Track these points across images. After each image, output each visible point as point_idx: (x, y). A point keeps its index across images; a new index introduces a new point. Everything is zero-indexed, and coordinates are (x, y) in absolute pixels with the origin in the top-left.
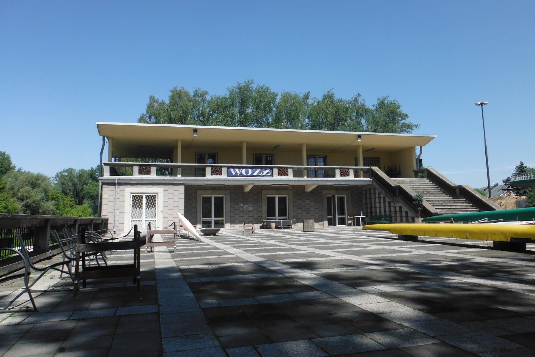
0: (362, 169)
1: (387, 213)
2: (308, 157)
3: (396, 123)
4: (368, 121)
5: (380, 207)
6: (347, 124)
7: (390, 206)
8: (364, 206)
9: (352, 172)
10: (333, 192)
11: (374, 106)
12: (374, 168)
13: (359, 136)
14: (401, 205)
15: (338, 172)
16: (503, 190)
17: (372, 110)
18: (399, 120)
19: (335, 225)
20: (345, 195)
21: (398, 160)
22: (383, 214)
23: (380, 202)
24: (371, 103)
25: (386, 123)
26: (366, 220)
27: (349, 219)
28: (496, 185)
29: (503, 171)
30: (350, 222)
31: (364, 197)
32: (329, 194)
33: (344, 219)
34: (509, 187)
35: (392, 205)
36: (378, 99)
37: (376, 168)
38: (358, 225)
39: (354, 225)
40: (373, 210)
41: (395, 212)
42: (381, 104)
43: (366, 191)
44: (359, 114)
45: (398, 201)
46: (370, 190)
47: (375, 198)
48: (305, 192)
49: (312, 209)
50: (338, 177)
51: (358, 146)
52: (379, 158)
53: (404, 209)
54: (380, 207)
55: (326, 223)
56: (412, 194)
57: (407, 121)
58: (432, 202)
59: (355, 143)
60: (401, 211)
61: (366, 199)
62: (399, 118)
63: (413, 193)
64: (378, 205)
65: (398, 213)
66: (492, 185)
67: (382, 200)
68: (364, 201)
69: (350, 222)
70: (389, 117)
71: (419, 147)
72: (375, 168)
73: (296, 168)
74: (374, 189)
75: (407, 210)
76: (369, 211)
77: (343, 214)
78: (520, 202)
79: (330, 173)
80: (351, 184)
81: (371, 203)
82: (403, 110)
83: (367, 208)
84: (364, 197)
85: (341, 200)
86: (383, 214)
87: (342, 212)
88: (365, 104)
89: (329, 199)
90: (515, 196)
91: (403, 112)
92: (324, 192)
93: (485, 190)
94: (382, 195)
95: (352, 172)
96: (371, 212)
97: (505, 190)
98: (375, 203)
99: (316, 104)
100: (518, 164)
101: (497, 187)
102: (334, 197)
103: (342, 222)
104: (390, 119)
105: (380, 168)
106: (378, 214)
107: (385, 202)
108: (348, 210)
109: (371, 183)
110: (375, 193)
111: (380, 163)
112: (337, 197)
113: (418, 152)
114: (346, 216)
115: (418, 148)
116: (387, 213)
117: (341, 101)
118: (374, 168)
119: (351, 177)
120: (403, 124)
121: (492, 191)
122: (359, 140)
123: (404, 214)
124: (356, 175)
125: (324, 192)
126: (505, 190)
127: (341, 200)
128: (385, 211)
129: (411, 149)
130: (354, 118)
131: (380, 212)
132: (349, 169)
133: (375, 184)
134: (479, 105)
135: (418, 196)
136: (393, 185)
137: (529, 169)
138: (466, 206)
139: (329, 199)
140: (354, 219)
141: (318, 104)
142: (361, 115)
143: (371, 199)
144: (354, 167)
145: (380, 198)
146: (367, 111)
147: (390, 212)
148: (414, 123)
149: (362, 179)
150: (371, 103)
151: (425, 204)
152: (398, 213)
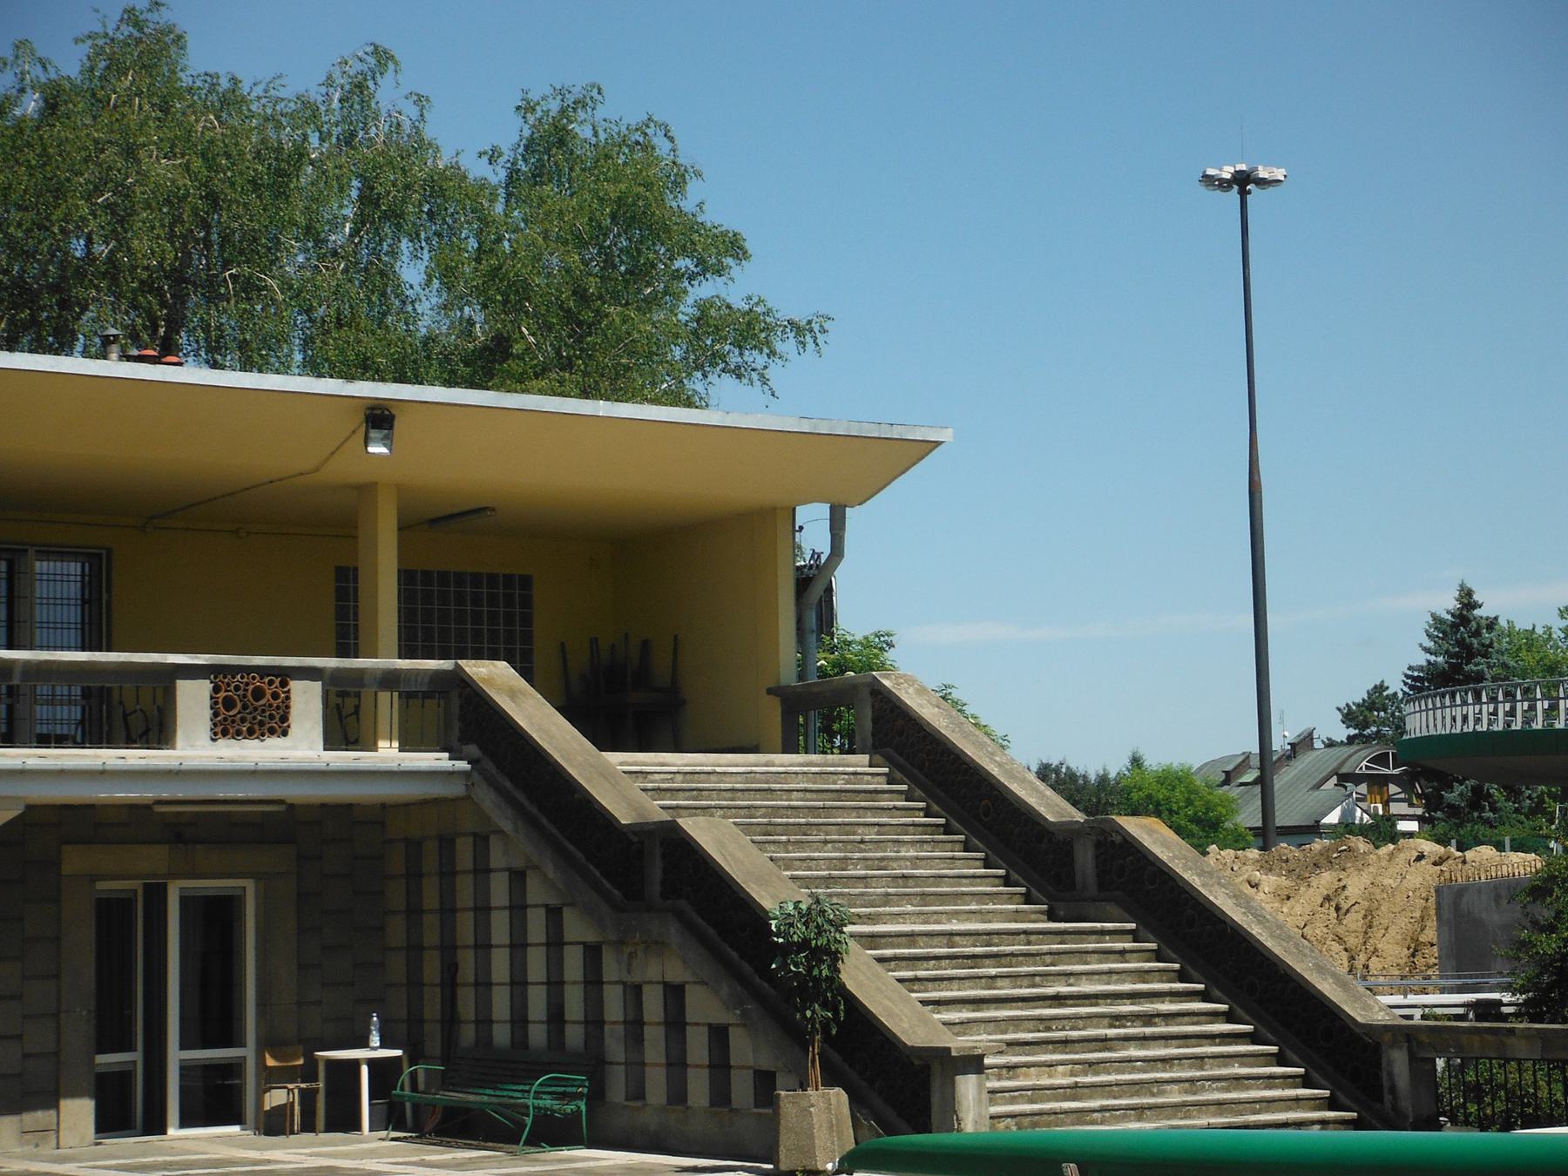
0: (390, 680)
1: (574, 1036)
2: (210, 1069)
3: (652, 302)
4: (445, 273)
5: (519, 983)
6: (286, 285)
7: (593, 981)
8: (397, 968)
9: (306, 701)
10: (153, 858)
11: (493, 156)
12: (480, 670)
13: (379, 418)
14: (675, 972)
15: (193, 699)
16: (1344, 778)
17: (482, 185)
18: (677, 276)
19: (156, 1125)
20: (249, 885)
21: (670, 613)
22: (538, 1035)
23: (518, 946)
24: (473, 135)
25: (581, 294)
26: (403, 1089)
27: (271, 1079)
28: (1304, 743)
29: (1354, 644)
30: (276, 1097)
31: (397, 896)
32: (119, 873)
33: (233, 1069)
34: (1381, 760)
35: (611, 968)
36: (526, 108)
38: (344, 1121)
39: (308, 1126)
41: (635, 1026)
42: (549, 146)
43: (414, 847)
44: (379, 213)
45: (657, 946)
46: (447, 843)
47: (483, 910)
50: (196, 746)
51: (365, 491)
52: (526, 582)
53: (703, 1006)
54: (519, 983)
55: (79, 1112)
56: (767, 903)
57: (734, 289)
58: (898, 955)
59: (345, 469)
60: (676, 1023)
61: (414, 912)
62: (682, 263)
63: (774, 891)
65: (654, 1036)
66: (1279, 744)
67: (536, 929)
68: (397, 932)
69: (276, 1097)
70: (601, 263)
71: (822, 511)
72: (494, 676)
74: (481, 841)
75: (721, 1016)
76: (432, 1008)
77: (230, 1037)
78: (1461, 891)
79: (139, 715)
81: (449, 949)
82: (711, 201)
83: (414, 983)
84: (397, 896)
85: (214, 922)
86: (538, 1035)
87: (214, 1019)
88: (429, 132)
90: (1429, 847)
91: (708, 218)
92: (74, 861)
93: (1228, 778)
94: (536, 892)
95: (306, 701)
96: (450, 1020)
97: (1356, 779)
98: (483, 946)
99: (31, 105)
100: (1446, 603)
101: (1305, 761)
102: (156, 895)
103: (215, 1101)
104: (609, 263)
105: (526, 674)
106: (502, 1035)
107: (555, 943)
108: (262, 1004)
109: (456, 789)
110: (482, 871)
111: (528, 638)
112: (185, 901)
113: (813, 535)
114: (248, 1052)
116: (574, 1036)
117: (230, 100)
118: (480, 670)
119: (301, 746)
120: (704, 307)
121: (1280, 781)
122: (377, 449)
123: (698, 1047)
124: (344, 729)
125: (74, 861)
126: (1356, 779)
127: (214, 922)
128: (556, 1016)
129: (772, 521)
130: (337, 239)
131: (519, 1020)
132: (286, 675)
133: (486, 798)
134: (1224, 185)
135: (807, 918)
136: (625, 818)
137: (1510, 632)
138: (1143, 975)
140: (309, 1073)
141: (52, 104)
142: (395, 216)
143: (448, 911)
145: (518, 909)
146: (443, 190)
147: (594, 1022)
148: (787, 305)
149: (387, 754)
150: (473, 135)
151: (864, 978)
152: (654, 1036)
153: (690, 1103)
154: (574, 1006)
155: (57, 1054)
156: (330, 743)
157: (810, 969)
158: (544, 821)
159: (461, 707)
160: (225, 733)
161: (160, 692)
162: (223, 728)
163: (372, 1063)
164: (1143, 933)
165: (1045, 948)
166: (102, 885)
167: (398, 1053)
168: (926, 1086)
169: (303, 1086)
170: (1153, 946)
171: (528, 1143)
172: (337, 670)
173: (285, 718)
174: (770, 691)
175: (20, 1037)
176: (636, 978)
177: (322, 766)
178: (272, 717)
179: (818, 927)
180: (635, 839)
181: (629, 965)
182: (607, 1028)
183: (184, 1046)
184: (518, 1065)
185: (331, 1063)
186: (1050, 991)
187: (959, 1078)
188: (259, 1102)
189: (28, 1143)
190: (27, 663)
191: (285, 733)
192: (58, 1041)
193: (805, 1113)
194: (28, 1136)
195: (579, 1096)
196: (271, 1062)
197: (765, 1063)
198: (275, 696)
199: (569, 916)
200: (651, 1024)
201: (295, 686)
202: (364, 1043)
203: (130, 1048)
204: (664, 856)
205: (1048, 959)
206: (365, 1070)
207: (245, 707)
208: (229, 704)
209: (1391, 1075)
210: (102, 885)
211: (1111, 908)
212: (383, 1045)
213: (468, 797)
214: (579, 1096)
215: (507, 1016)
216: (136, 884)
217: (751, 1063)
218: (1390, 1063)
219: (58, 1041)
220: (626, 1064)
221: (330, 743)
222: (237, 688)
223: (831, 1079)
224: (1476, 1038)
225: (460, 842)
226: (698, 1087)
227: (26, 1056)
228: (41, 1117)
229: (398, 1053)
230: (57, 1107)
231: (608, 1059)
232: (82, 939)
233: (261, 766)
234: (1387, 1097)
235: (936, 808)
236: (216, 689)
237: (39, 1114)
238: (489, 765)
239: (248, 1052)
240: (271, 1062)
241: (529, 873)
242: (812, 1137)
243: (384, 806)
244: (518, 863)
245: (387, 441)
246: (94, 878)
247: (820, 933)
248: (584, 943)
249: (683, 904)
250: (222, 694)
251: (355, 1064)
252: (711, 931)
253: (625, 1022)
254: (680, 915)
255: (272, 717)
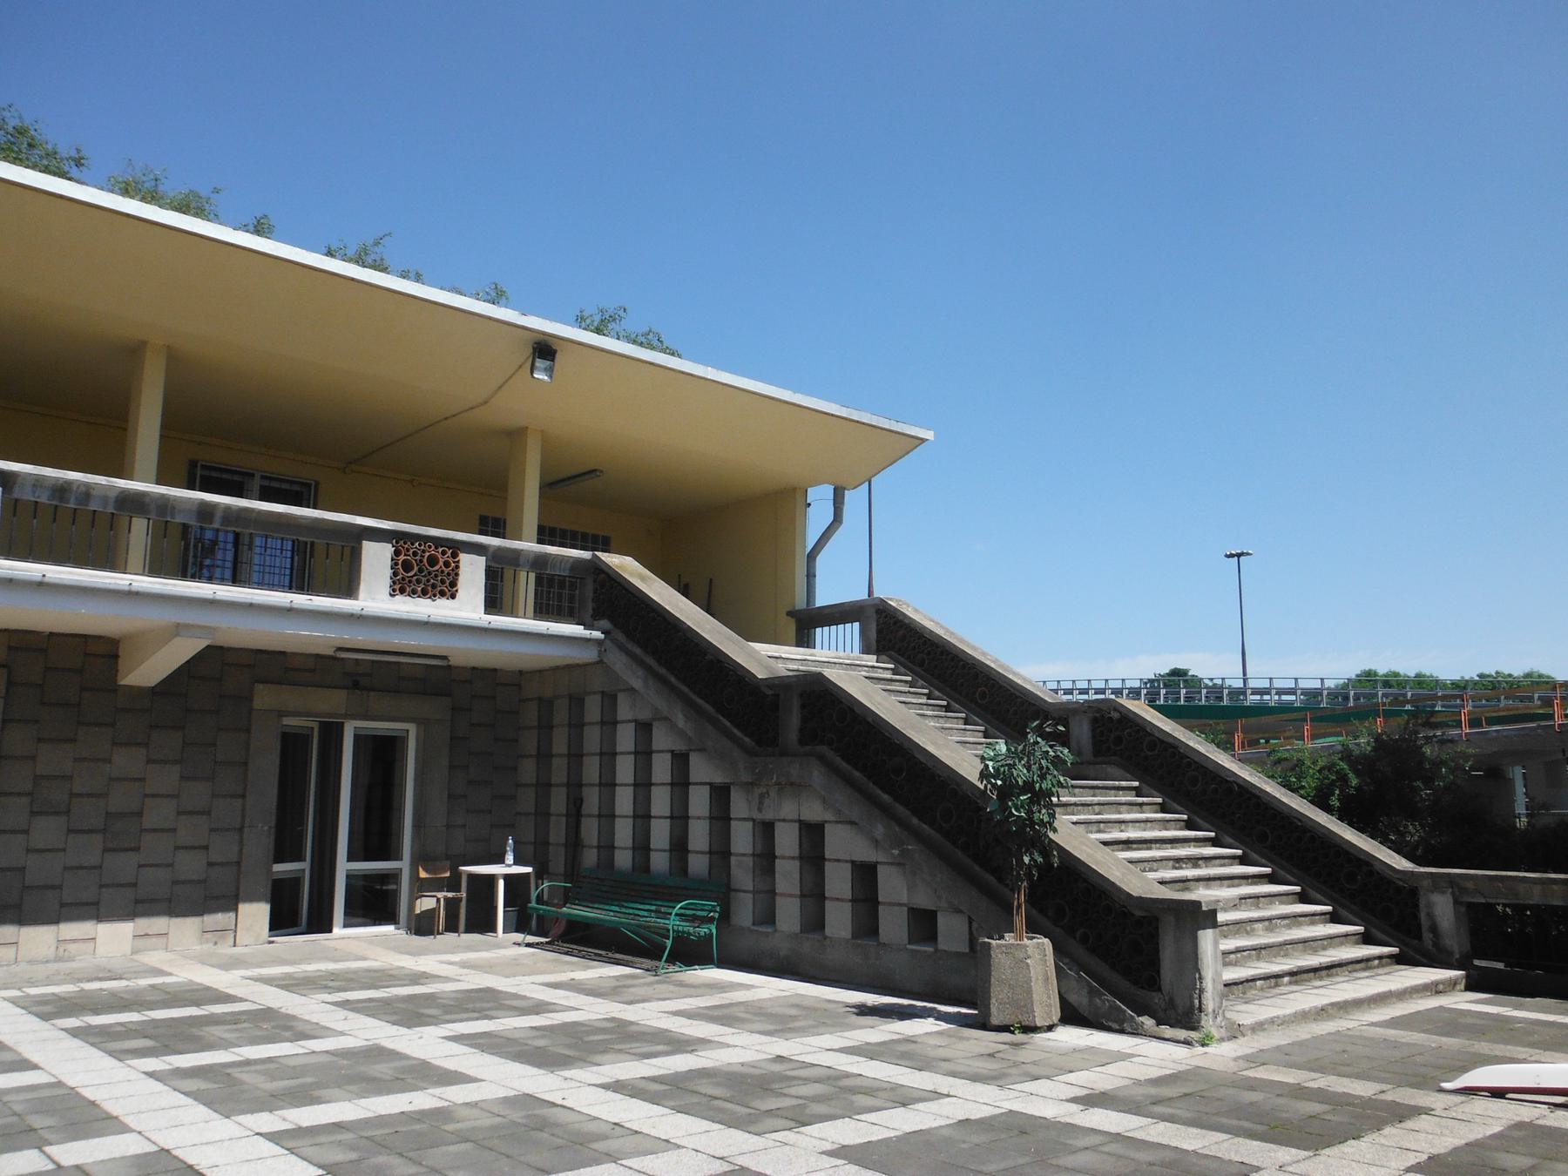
1: (698, 864)
2: (368, 877)
5: (642, 816)
7: (721, 817)
8: (527, 801)
9: (472, 571)
10: (330, 701)
12: (613, 560)
14: (813, 811)
15: (376, 559)
19: (321, 923)
20: (412, 729)
23: (643, 785)
27: (421, 888)
30: (426, 904)
31: (530, 743)
32: (302, 710)
35: (740, 805)
37: (628, 560)
38: (482, 923)
39: (452, 927)
40: (590, 831)
41: (766, 859)
43: (546, 705)
45: (795, 787)
46: (577, 702)
47: (609, 756)
48: (112, 688)
49: (159, 814)
50: (375, 596)
53: (844, 845)
54: (642, 816)
55: (256, 914)
61: (544, 756)
64: (624, 801)
65: (788, 875)
67: (662, 769)
68: (528, 771)
69: (426, 904)
71: (827, 491)
73: (38, 481)
74: (610, 699)
75: (865, 853)
76: (557, 832)
79: (323, 563)
80: (464, 651)
81: (575, 787)
84: (530, 743)
85: (381, 756)
86: (660, 861)
87: (376, 837)
89: (293, 745)
92: (265, 698)
94: (662, 739)
95: (472, 571)
96: (574, 844)
102: (332, 734)
103: (374, 904)
106: (624, 859)
107: (681, 784)
108: (417, 826)
109: (590, 655)
110: (610, 723)
112: (358, 739)
114: (403, 865)
115: (820, 500)
116: (698, 864)
118: (613, 560)
119: (466, 605)
123: (839, 882)
125: (265, 698)
127: (381, 756)
128: (679, 846)
129: (784, 501)
131: (642, 847)
132: (457, 547)
139: (293, 745)
140: (453, 884)
143: (576, 756)
144: (494, 542)
145: (644, 754)
147: (721, 852)
152: (788, 875)
153: (828, 931)
154: (699, 835)
155: (238, 863)
156: (487, 612)
157: (1030, 812)
158: (673, 679)
159: (595, 591)
160: (402, 591)
161: (347, 551)
162: (401, 585)
163: (507, 878)
164: (1146, 789)
165: (1096, 799)
166: (287, 721)
167: (529, 870)
168: (1153, 938)
169: (450, 895)
170: (1160, 800)
171: (672, 960)
172: (499, 549)
173: (453, 584)
174: (789, 614)
175: (206, 848)
176: (768, 815)
177: (485, 625)
178: (443, 582)
179: (1041, 768)
180: (770, 692)
181: (761, 803)
182: (733, 859)
183: (351, 857)
184: (639, 885)
185: (471, 876)
186: (1124, 836)
187: (1200, 933)
188: (411, 907)
189: (207, 941)
190: (228, 508)
191: (453, 597)
192: (241, 851)
193: (1022, 964)
194: (209, 935)
195: (711, 920)
196: (423, 874)
197: (924, 901)
198: (447, 564)
199: (694, 759)
200: (783, 858)
201: (464, 558)
202: (500, 859)
203: (299, 858)
204: (803, 706)
205: (1097, 808)
206: (501, 883)
207: (421, 571)
208: (407, 566)
209: (1430, 916)
210: (287, 721)
211: (1111, 770)
212: (516, 862)
213: (601, 662)
214: (711, 920)
215: (629, 843)
216: (312, 723)
217: (905, 900)
218: (1430, 905)
219: (241, 851)
220: (754, 892)
221: (487, 612)
222: (415, 554)
223: (1033, 928)
224: (1539, 887)
225: (588, 700)
226: (839, 920)
227: (210, 864)
228: (220, 919)
229: (529, 870)
230: (236, 910)
231: (733, 886)
232: (267, 765)
233: (432, 619)
234: (1427, 936)
235: (937, 693)
236: (397, 553)
237: (220, 916)
238: (621, 637)
239: (403, 865)
240: (423, 874)
241: (656, 724)
242: (1029, 992)
243: (521, 672)
244: (644, 715)
245: (550, 371)
246: (282, 714)
247: (1043, 777)
248: (710, 784)
249: (824, 749)
250: (402, 558)
251: (491, 879)
252: (857, 774)
253: (753, 855)
254: (822, 758)
255: (443, 582)
